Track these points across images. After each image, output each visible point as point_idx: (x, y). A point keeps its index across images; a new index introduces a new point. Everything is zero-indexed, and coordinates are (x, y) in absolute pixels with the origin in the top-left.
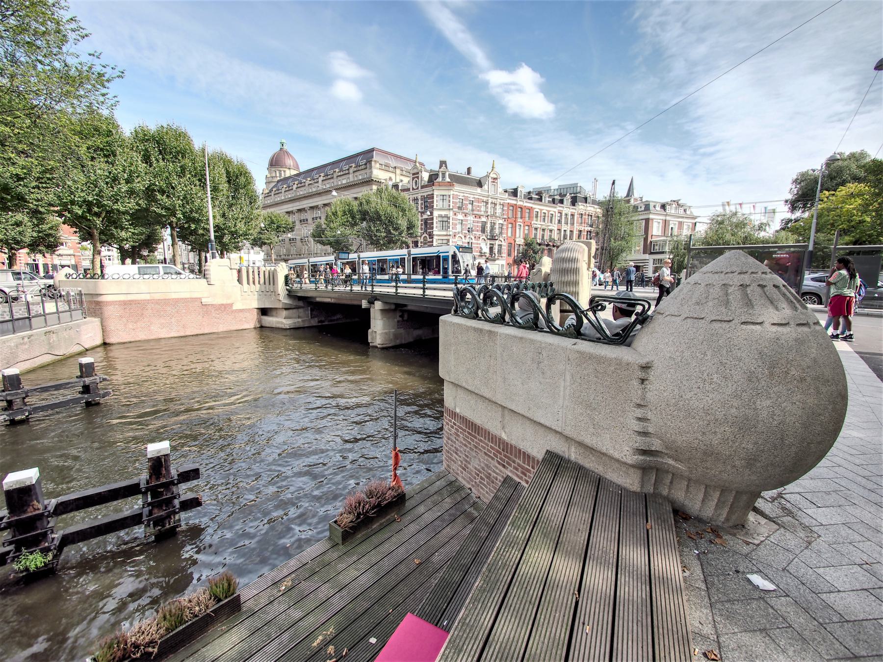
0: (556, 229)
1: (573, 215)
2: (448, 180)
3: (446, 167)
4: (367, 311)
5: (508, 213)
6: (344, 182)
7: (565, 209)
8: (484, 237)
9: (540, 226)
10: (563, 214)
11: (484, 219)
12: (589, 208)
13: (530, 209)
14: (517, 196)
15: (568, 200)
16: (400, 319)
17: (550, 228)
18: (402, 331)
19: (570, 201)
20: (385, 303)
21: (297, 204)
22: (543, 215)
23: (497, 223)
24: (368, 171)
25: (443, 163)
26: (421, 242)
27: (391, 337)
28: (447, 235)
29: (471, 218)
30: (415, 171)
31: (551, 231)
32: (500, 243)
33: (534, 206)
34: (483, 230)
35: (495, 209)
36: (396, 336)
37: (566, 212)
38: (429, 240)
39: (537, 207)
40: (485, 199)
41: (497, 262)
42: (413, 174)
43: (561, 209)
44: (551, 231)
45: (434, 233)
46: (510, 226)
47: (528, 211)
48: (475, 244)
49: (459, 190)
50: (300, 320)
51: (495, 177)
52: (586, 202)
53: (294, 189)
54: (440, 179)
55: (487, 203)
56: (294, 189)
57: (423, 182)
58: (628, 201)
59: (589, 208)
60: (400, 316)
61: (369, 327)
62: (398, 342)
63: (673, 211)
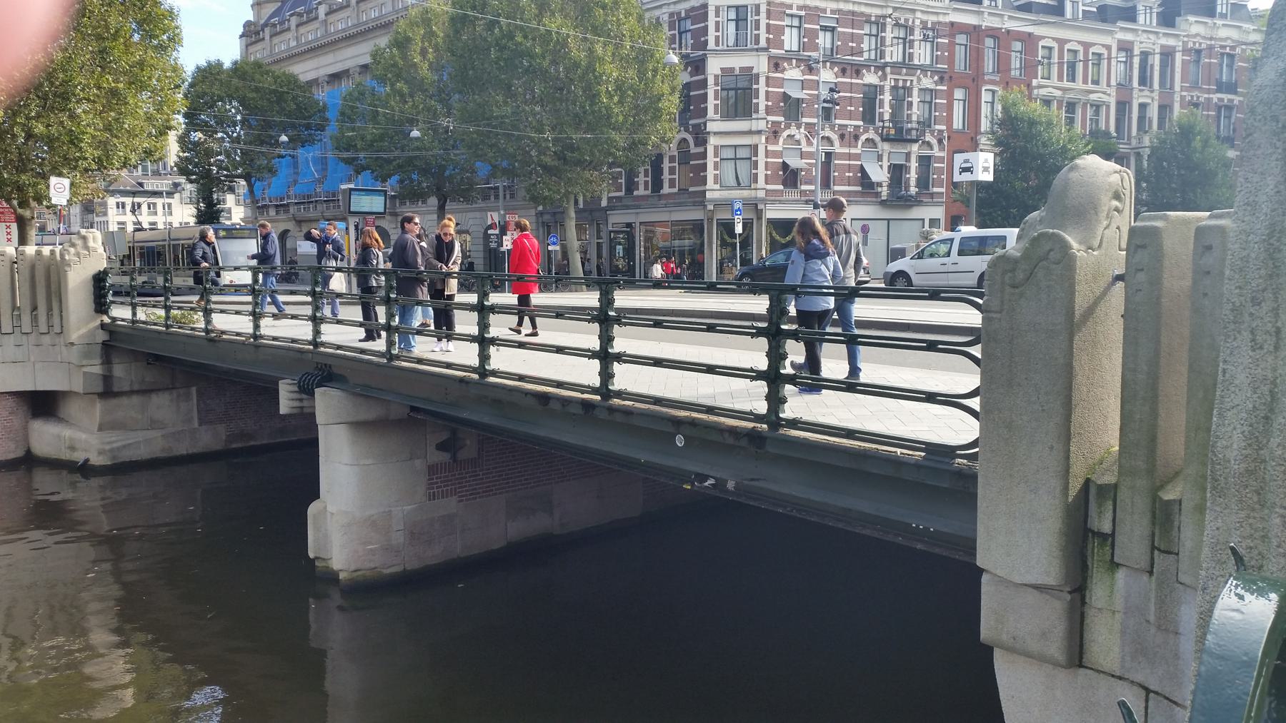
5: (952, 54)
7: (1143, 37)
8: (871, 134)
9: (1058, 93)
10: (1137, 52)
11: (870, 78)
13: (1029, 41)
16: (444, 457)
17: (1093, 97)
18: (450, 505)
21: (329, 58)
26: (672, 159)
27: (398, 538)
28: (750, 132)
31: (1097, 107)
32: (927, 152)
34: (869, 114)
35: (907, 43)
36: (415, 534)
37: (1146, 47)
38: (694, 150)
41: (917, 212)
43: (1129, 37)
45: (711, 127)
47: (1017, 46)
48: (842, 156)
53: (293, 27)
56: (293, 27)
59: (1223, 33)
60: (441, 447)
61: (315, 494)
62: (434, 554)
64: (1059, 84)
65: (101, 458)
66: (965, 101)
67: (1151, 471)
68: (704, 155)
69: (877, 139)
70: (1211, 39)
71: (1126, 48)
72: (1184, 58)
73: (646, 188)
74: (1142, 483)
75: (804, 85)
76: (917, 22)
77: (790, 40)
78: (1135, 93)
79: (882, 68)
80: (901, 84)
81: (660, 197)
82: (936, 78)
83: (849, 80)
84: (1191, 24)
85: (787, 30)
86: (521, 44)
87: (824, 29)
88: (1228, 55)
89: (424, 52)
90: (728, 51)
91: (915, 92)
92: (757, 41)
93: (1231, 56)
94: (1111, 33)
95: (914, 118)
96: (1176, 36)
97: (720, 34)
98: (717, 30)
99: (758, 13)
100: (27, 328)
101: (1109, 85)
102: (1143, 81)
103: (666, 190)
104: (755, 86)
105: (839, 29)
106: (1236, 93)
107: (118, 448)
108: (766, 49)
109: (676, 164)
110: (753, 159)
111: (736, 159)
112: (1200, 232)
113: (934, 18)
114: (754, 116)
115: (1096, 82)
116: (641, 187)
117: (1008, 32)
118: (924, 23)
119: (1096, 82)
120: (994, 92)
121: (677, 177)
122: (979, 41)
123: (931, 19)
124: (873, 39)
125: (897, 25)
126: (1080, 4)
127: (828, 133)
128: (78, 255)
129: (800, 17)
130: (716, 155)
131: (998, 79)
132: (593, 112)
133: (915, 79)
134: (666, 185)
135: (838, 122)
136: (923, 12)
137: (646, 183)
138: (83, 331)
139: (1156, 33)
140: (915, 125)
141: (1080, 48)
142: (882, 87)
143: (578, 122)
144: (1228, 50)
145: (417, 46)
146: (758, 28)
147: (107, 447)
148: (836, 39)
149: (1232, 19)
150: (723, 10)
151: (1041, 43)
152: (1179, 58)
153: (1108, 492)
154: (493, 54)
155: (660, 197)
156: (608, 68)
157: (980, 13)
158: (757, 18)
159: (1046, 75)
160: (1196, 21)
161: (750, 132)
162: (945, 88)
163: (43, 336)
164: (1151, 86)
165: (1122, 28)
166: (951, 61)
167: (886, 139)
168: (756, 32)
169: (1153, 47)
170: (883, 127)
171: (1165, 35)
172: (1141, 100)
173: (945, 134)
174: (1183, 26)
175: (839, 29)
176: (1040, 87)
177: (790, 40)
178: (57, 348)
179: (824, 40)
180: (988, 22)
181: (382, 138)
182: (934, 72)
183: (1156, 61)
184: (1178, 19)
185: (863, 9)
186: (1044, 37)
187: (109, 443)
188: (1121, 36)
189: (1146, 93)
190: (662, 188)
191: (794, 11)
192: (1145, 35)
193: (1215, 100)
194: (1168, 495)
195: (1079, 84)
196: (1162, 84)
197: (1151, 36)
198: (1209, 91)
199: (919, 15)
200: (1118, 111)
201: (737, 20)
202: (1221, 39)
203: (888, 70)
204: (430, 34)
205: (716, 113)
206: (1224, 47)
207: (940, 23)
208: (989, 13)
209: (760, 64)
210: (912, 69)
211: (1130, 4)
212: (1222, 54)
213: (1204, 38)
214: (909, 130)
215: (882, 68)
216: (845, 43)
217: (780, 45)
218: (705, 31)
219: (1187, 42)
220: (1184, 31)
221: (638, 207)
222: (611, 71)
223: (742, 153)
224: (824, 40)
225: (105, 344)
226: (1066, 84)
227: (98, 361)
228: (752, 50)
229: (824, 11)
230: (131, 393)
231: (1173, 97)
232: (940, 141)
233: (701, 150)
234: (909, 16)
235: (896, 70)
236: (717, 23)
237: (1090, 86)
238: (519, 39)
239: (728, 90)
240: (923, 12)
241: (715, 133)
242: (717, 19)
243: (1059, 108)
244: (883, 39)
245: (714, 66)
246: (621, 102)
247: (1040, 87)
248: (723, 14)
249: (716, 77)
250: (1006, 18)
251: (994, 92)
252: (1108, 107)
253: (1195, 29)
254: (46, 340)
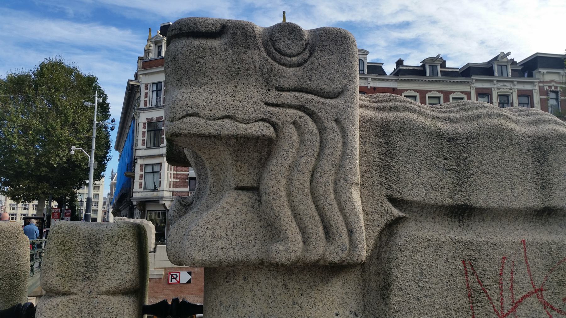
7: (500, 85)
45: (139, 153)
72: (541, 97)
84: (543, 74)
90: (152, 108)
94: (468, 83)
112: (133, 218)
126: (439, 67)
130: (141, 170)
139: (512, 82)
141: (442, 96)
150: (150, 85)
160: (547, 72)
165: (477, 80)
169: (511, 91)
171: (519, 82)
201: (157, 91)
202: (547, 82)
205: (143, 144)
208: (372, 78)
219: (543, 86)
220: (538, 79)
241: (141, 157)
242: (146, 91)
250: (370, 80)
253: (548, 78)
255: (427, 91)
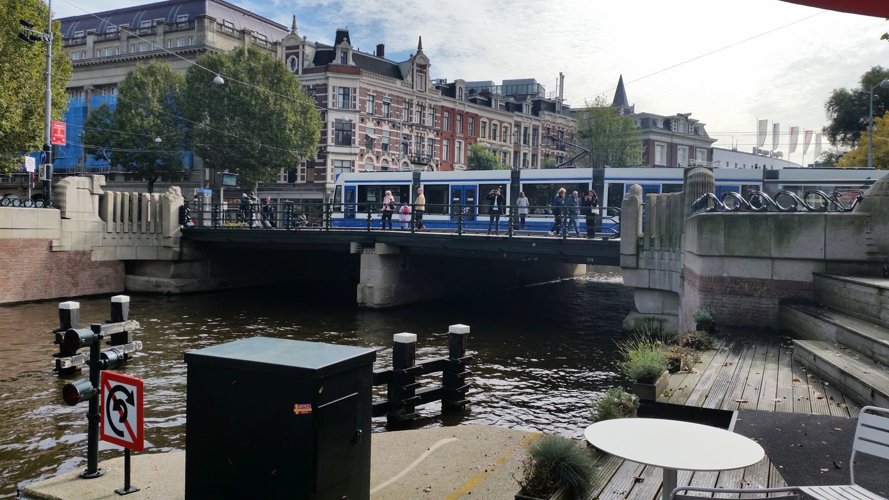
0: (512, 151)
1: (535, 129)
2: (351, 62)
3: (348, 41)
4: (356, 260)
5: (442, 122)
6: (107, 53)
8: (406, 160)
9: (489, 145)
11: (406, 131)
12: (559, 121)
13: (476, 117)
14: (454, 96)
15: (527, 108)
17: (504, 148)
19: (531, 107)
20: (389, 244)
22: (503, 130)
23: (426, 137)
24: (194, 34)
25: (342, 36)
27: (393, 294)
28: (350, 154)
29: (386, 127)
30: (292, 43)
33: (480, 113)
35: (422, 114)
37: (526, 125)
39: (484, 114)
40: (408, 97)
42: (288, 48)
43: (519, 119)
44: (505, 153)
45: (329, 149)
46: (445, 142)
49: (367, 82)
50: (195, 280)
51: (423, 63)
52: (554, 112)
54: (338, 61)
55: (410, 104)
57: (306, 64)
58: (617, 112)
59: (559, 121)
63: (681, 130)
64: (489, 141)
65: (176, 289)
66: (447, 146)
67: (650, 234)
68: (325, 164)
69: (409, 162)
70: (554, 123)
71: (518, 125)
73: (285, 180)
74: (648, 236)
75: (375, 131)
76: (427, 105)
77: (369, 108)
78: (522, 149)
79: (411, 126)
80: (419, 135)
81: (295, 185)
82: (435, 133)
83: (396, 131)
85: (368, 102)
86: (242, 98)
87: (385, 103)
88: (561, 131)
89: (153, 92)
91: (426, 140)
92: (355, 107)
93: (562, 132)
94: (512, 117)
95: (426, 153)
96: (539, 120)
97: (335, 101)
98: (334, 99)
99: (355, 92)
100: (135, 230)
101: (510, 143)
102: (525, 142)
103: (299, 181)
104: (353, 130)
105: (392, 104)
106: (564, 151)
107: (183, 286)
108: (359, 112)
109: (305, 168)
110: (352, 168)
111: (342, 167)
113: (434, 103)
114: (353, 145)
115: (505, 141)
116: (282, 179)
117: (467, 112)
118: (430, 105)
119: (505, 141)
120: (460, 142)
121: (305, 174)
122: (454, 117)
123: (434, 103)
124: (406, 110)
125: (418, 105)
127: (386, 157)
128: (174, 198)
129: (373, 96)
131: (462, 136)
132: (282, 138)
133: (426, 133)
134: (299, 179)
135: (391, 152)
136: (430, 99)
137: (285, 177)
138: (175, 232)
139: (531, 118)
140: (426, 157)
142: (411, 136)
143: (272, 141)
144: (561, 129)
145: (149, 89)
146: (355, 100)
147: (179, 285)
148: (390, 109)
149: (563, 114)
151: (482, 120)
152: (540, 131)
153: (642, 239)
154: (226, 101)
155: (295, 185)
156: (290, 115)
157: (454, 102)
158: (354, 95)
159: (483, 136)
161: (350, 154)
162: (439, 139)
163: (125, 234)
164: (528, 145)
165: (517, 115)
166: (442, 126)
167: (413, 163)
168: (354, 102)
170: (412, 156)
172: (525, 151)
173: (439, 162)
174: (543, 116)
175: (392, 104)
176: (481, 142)
177: (369, 108)
178: (150, 240)
179: (384, 109)
180: (459, 107)
181: (129, 140)
182: (435, 130)
183: (530, 131)
184: (540, 112)
185: (402, 95)
186: (483, 117)
187: (179, 283)
188: (516, 119)
189: (527, 148)
190: (296, 180)
191: (371, 93)
192: (526, 119)
193: (556, 154)
194: (652, 237)
195: (497, 142)
196: (533, 143)
197: (529, 120)
198: (553, 149)
199: (428, 101)
200: (514, 155)
201: (344, 95)
202: (558, 124)
203: (414, 127)
204: (156, 81)
205: (332, 142)
206: (559, 128)
207: (437, 106)
209: (355, 118)
210: (425, 128)
211: (519, 103)
212: (559, 131)
213: (551, 122)
214: (423, 159)
215: (411, 126)
216: (394, 112)
217: (365, 110)
218: (326, 98)
221: (280, 190)
222: (292, 118)
223: (346, 164)
224: (384, 109)
225: (181, 238)
226: (492, 141)
227: (178, 246)
228: (352, 111)
229: (385, 94)
230: (187, 261)
231: (538, 151)
232: (437, 166)
233: (322, 161)
234: (424, 101)
235: (418, 128)
236: (334, 95)
237: (503, 143)
238: (242, 94)
239: (339, 130)
240: (430, 99)
241: (332, 153)
243: (500, 154)
244: (424, 114)
245: (332, 117)
246: (295, 134)
247: (481, 142)
248: (337, 90)
249: (333, 123)
250: (466, 106)
251: (460, 142)
252: (510, 153)
254: (144, 236)
255: (298, 57)
